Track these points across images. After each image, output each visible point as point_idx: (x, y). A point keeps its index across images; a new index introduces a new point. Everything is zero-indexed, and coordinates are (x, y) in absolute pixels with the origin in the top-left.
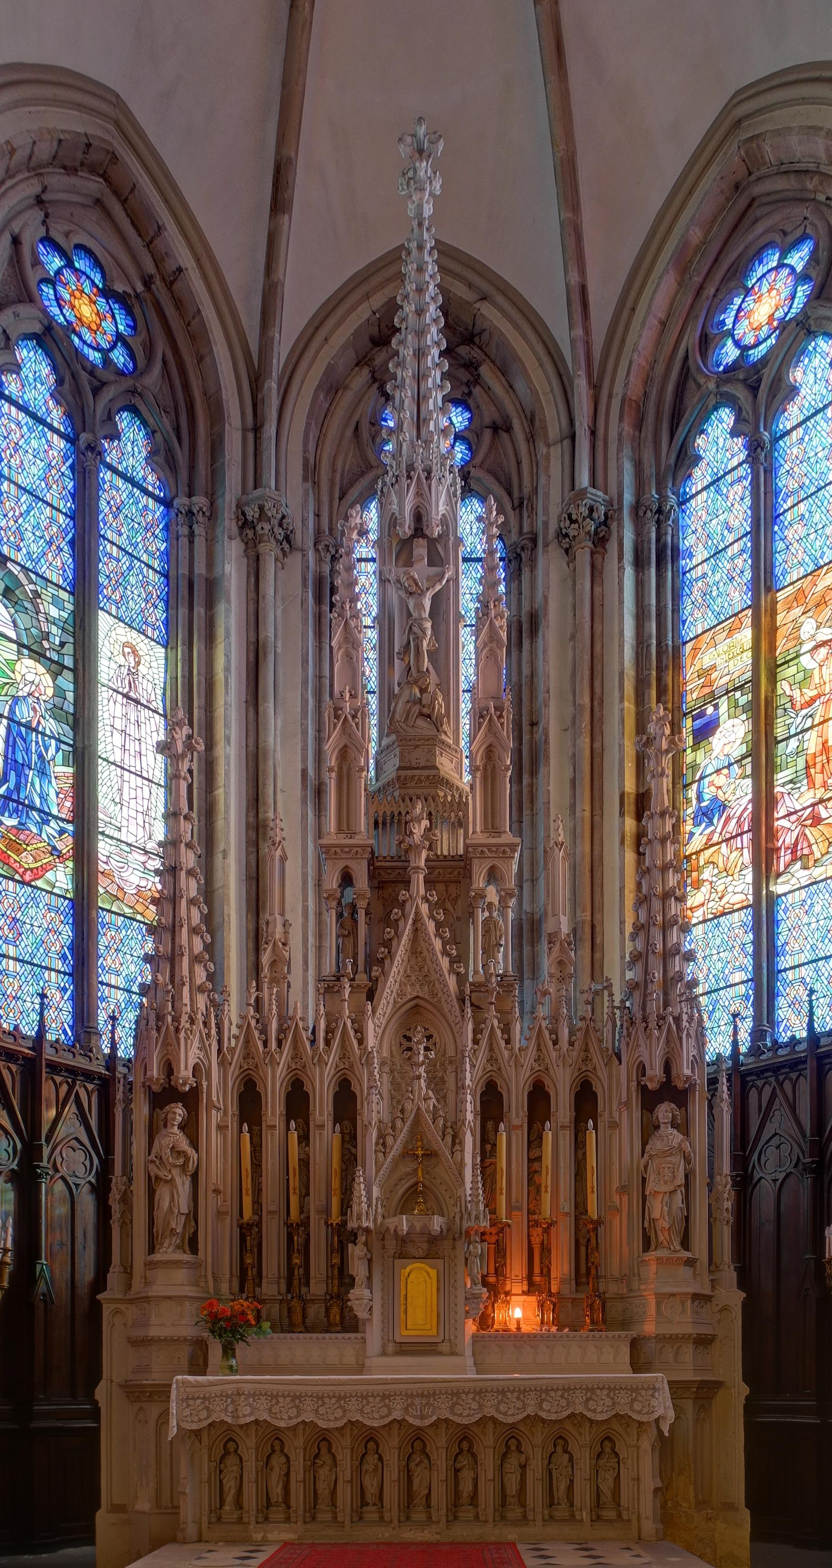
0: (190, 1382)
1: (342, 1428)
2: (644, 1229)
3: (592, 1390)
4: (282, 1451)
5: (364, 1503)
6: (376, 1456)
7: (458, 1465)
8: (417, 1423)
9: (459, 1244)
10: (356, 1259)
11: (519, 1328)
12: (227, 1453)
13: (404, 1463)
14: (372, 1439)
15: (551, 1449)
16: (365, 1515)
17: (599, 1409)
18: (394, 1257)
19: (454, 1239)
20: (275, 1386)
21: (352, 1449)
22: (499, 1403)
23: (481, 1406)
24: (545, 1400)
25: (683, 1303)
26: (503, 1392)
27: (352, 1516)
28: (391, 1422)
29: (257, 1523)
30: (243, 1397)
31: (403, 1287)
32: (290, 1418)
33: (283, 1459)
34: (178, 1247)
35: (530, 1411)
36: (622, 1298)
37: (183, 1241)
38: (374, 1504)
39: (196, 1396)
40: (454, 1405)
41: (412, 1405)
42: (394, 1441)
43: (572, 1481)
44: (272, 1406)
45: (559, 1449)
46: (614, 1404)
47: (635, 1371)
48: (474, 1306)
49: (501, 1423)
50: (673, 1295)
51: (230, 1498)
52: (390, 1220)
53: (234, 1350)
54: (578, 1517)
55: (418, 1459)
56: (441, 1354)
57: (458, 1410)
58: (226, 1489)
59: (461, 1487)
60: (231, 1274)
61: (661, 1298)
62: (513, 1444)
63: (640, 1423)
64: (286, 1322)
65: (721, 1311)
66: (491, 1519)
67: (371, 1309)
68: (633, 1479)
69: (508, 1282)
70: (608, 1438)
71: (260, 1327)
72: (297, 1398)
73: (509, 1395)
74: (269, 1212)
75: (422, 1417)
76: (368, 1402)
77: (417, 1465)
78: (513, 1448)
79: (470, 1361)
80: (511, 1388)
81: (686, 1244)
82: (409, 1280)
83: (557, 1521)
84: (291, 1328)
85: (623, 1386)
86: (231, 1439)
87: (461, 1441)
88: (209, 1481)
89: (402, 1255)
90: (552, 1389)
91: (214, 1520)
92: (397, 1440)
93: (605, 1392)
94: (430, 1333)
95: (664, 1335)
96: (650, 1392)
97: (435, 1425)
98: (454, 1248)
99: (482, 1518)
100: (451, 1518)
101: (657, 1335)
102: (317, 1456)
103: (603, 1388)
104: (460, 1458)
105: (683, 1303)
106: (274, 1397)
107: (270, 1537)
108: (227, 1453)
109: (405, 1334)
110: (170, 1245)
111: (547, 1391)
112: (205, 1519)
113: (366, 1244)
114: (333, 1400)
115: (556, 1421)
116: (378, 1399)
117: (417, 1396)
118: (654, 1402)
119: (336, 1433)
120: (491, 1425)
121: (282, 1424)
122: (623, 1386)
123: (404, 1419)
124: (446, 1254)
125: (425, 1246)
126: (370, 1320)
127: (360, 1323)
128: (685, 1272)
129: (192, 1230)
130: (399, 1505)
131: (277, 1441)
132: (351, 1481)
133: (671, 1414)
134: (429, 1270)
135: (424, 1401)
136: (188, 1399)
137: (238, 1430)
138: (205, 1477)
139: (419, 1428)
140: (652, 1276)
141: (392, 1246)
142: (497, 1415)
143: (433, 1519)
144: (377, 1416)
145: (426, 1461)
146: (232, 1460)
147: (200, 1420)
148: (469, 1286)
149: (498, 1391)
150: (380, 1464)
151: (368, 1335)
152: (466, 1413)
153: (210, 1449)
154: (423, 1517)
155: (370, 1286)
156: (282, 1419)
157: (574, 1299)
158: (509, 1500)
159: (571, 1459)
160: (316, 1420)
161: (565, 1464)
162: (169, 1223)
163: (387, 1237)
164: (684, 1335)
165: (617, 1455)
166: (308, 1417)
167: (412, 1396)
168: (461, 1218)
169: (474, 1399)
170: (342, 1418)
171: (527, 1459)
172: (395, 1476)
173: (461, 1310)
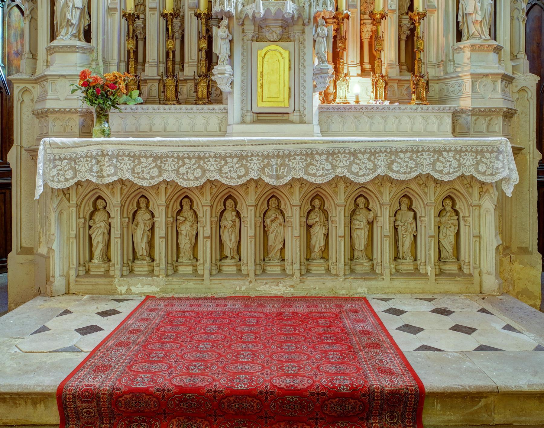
0: (56, 144)
1: (202, 187)
2: (458, 23)
3: (440, 152)
4: (147, 207)
5: (223, 257)
6: (234, 213)
7: (310, 222)
8: (273, 182)
9: (307, 29)
10: (219, 39)
11: (357, 102)
12: (96, 209)
13: (260, 220)
14: (230, 197)
15: (397, 207)
16: (224, 269)
17: (446, 171)
18: (252, 41)
19: (304, 25)
20: (138, 148)
21: (212, 207)
22: (351, 164)
23: (333, 167)
24: (311, 164)
25: (494, 82)
26: (354, 154)
27: (211, 270)
28: (249, 182)
29: (122, 276)
30: (107, 158)
31: (260, 66)
32: (152, 178)
33: (148, 216)
34: (74, 36)
35: (380, 171)
36: (439, 80)
37: (79, 32)
38: (233, 258)
39: (63, 156)
40: (308, 165)
41: (268, 165)
42: (251, 199)
43: (415, 237)
44: (135, 166)
45: (404, 207)
46: (460, 165)
47: (455, 136)
48: (321, 80)
49: (352, 182)
50: (486, 75)
51: (98, 252)
52: (248, 7)
53: (106, 116)
54: (422, 271)
55: (273, 216)
56: (292, 122)
57: (312, 170)
58: (94, 243)
59: (313, 242)
60: (120, 60)
61: (475, 77)
62: (361, 202)
63: (482, 183)
64: (162, 98)
65: (519, 91)
66: (341, 273)
67: (232, 83)
68: (475, 237)
69: (346, 67)
70: (449, 197)
71: (131, 96)
72: (157, 158)
73: (360, 156)
74: (151, 9)
75: (278, 177)
76: (226, 163)
77: (272, 221)
78: (362, 205)
79: (317, 129)
80: (363, 150)
81: (493, 34)
82: (266, 59)
83: (403, 274)
84: (165, 101)
85: (469, 149)
86: (99, 197)
87: (313, 200)
88: (77, 237)
89: (259, 38)
90: (402, 151)
91: (82, 273)
92: (253, 198)
93: (452, 154)
94: (282, 105)
95: (479, 109)
96: (494, 155)
97: (290, 185)
98: (303, 32)
99: (333, 272)
100: (304, 272)
101: (474, 109)
102: (179, 213)
103: (450, 150)
104: (312, 215)
105: (494, 82)
106: (136, 158)
107: (134, 289)
108: (96, 209)
109: (260, 105)
110: (67, 33)
111: (396, 153)
112: (73, 273)
113: (228, 27)
114: (193, 161)
115: (402, 182)
116: (236, 160)
117: (273, 156)
118: (498, 164)
119: (196, 192)
120: (342, 185)
121: (145, 184)
122: (469, 149)
123: (260, 179)
124: (296, 37)
125: (279, 30)
126: (231, 93)
127: (224, 98)
128: (492, 57)
129: (87, 23)
130: (255, 260)
131: (142, 199)
132: (211, 237)
133: (515, 176)
134: (282, 51)
135: (280, 162)
136: (55, 159)
137: (104, 189)
138: (73, 233)
139: (274, 187)
140: (466, 61)
141: (250, 29)
142: (349, 175)
143: (287, 272)
144: (234, 175)
145: (281, 217)
146: (100, 217)
147: (67, 180)
148: (316, 63)
149: (350, 153)
150: (238, 221)
151: (229, 106)
152: (319, 173)
153: (78, 206)
154: (278, 270)
155: (231, 64)
156: (144, 178)
157: (400, 80)
158: (356, 254)
159: (415, 217)
160: (177, 180)
161: (410, 221)
162: (65, 15)
163: (246, 23)
164: (485, 109)
165: (457, 213)
166: (169, 176)
167: (268, 157)
168: (310, 6)
169: (327, 160)
170: (201, 178)
171: (376, 217)
172: (252, 233)
173: (309, 84)
